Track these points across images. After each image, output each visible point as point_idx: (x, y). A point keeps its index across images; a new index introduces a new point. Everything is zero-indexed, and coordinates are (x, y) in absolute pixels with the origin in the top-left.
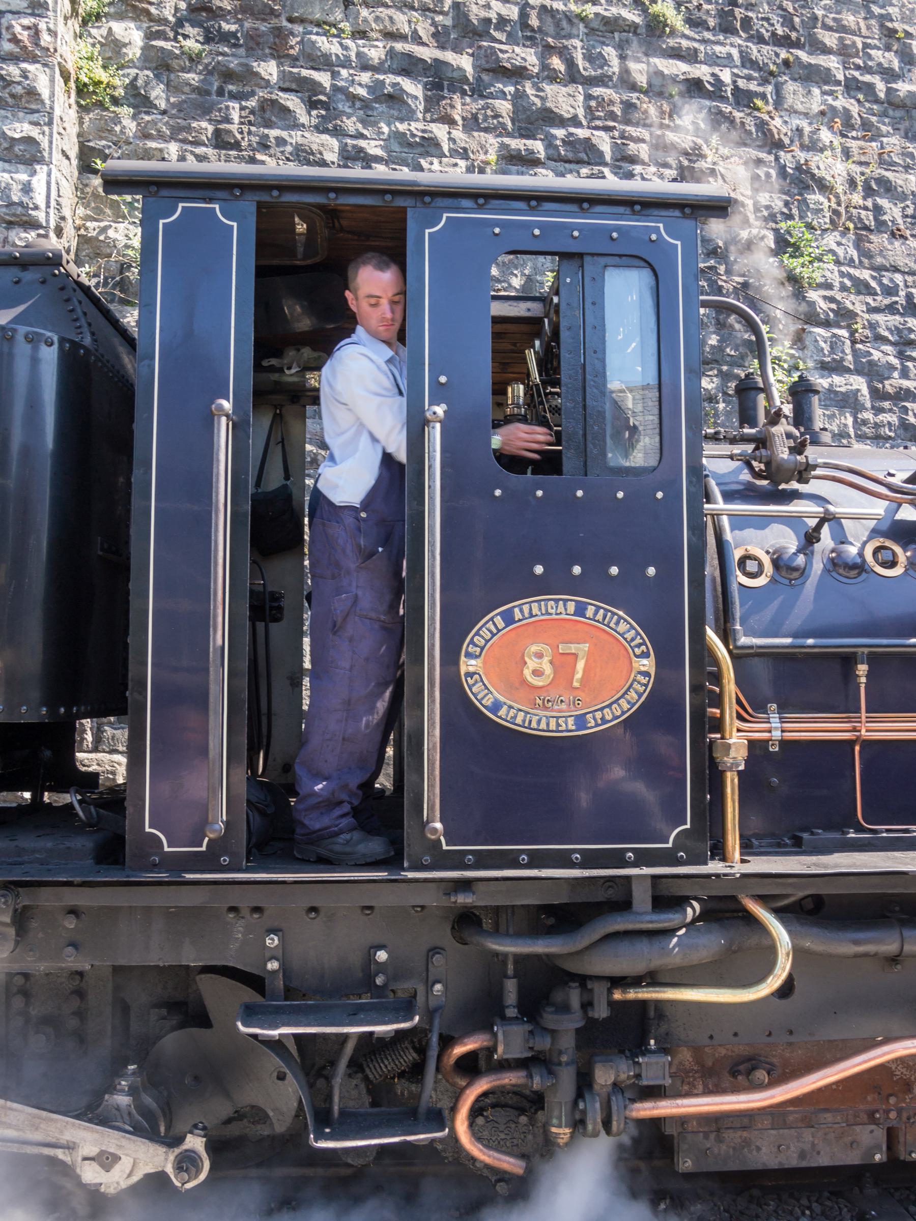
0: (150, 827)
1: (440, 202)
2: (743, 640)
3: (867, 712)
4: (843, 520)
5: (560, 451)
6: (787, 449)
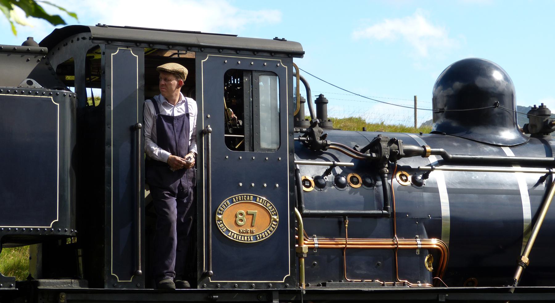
0: (113, 273)
1: (207, 50)
2: (305, 211)
3: (348, 238)
4: (514, 156)
5: (225, 134)
6: (319, 138)
